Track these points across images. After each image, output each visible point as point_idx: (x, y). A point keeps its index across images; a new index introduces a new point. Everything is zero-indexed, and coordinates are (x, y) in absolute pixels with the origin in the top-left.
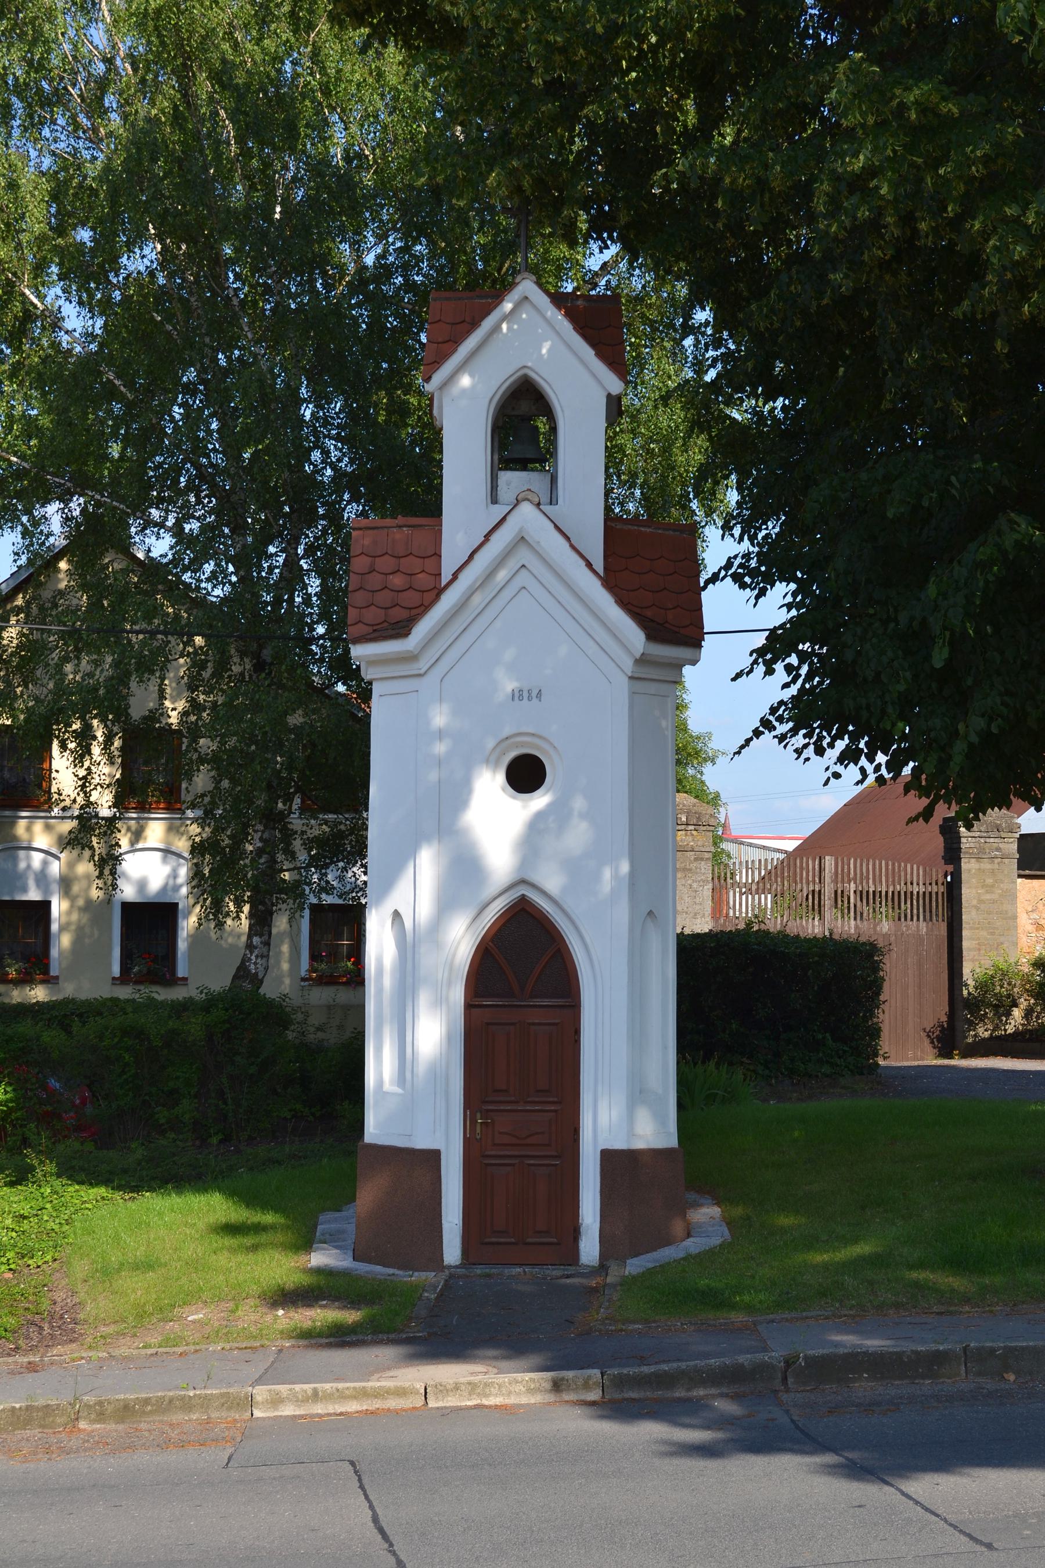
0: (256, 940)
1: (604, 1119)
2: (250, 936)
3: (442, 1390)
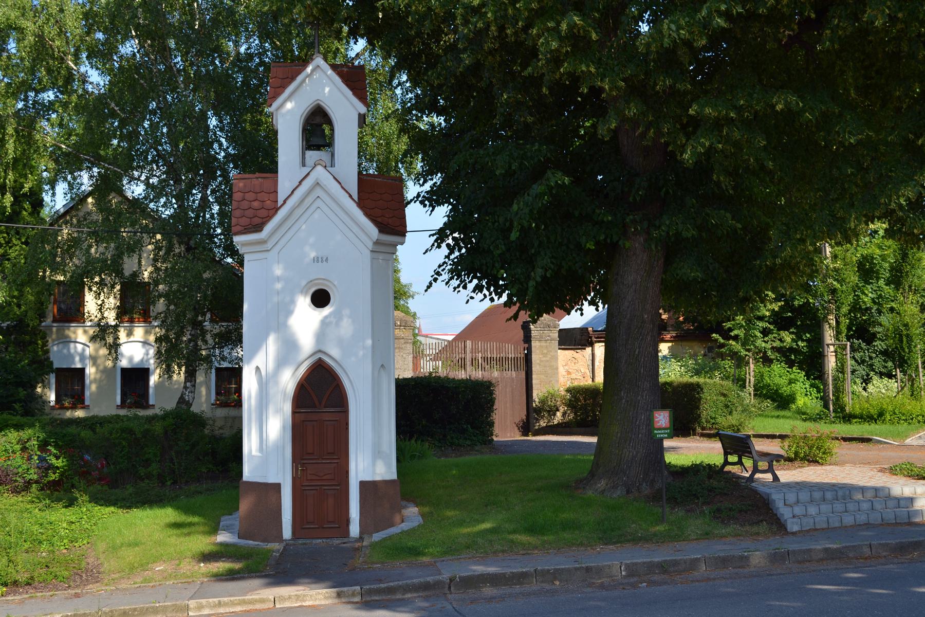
0: (188, 384)
1: (361, 466)
2: (185, 382)
3: (283, 599)
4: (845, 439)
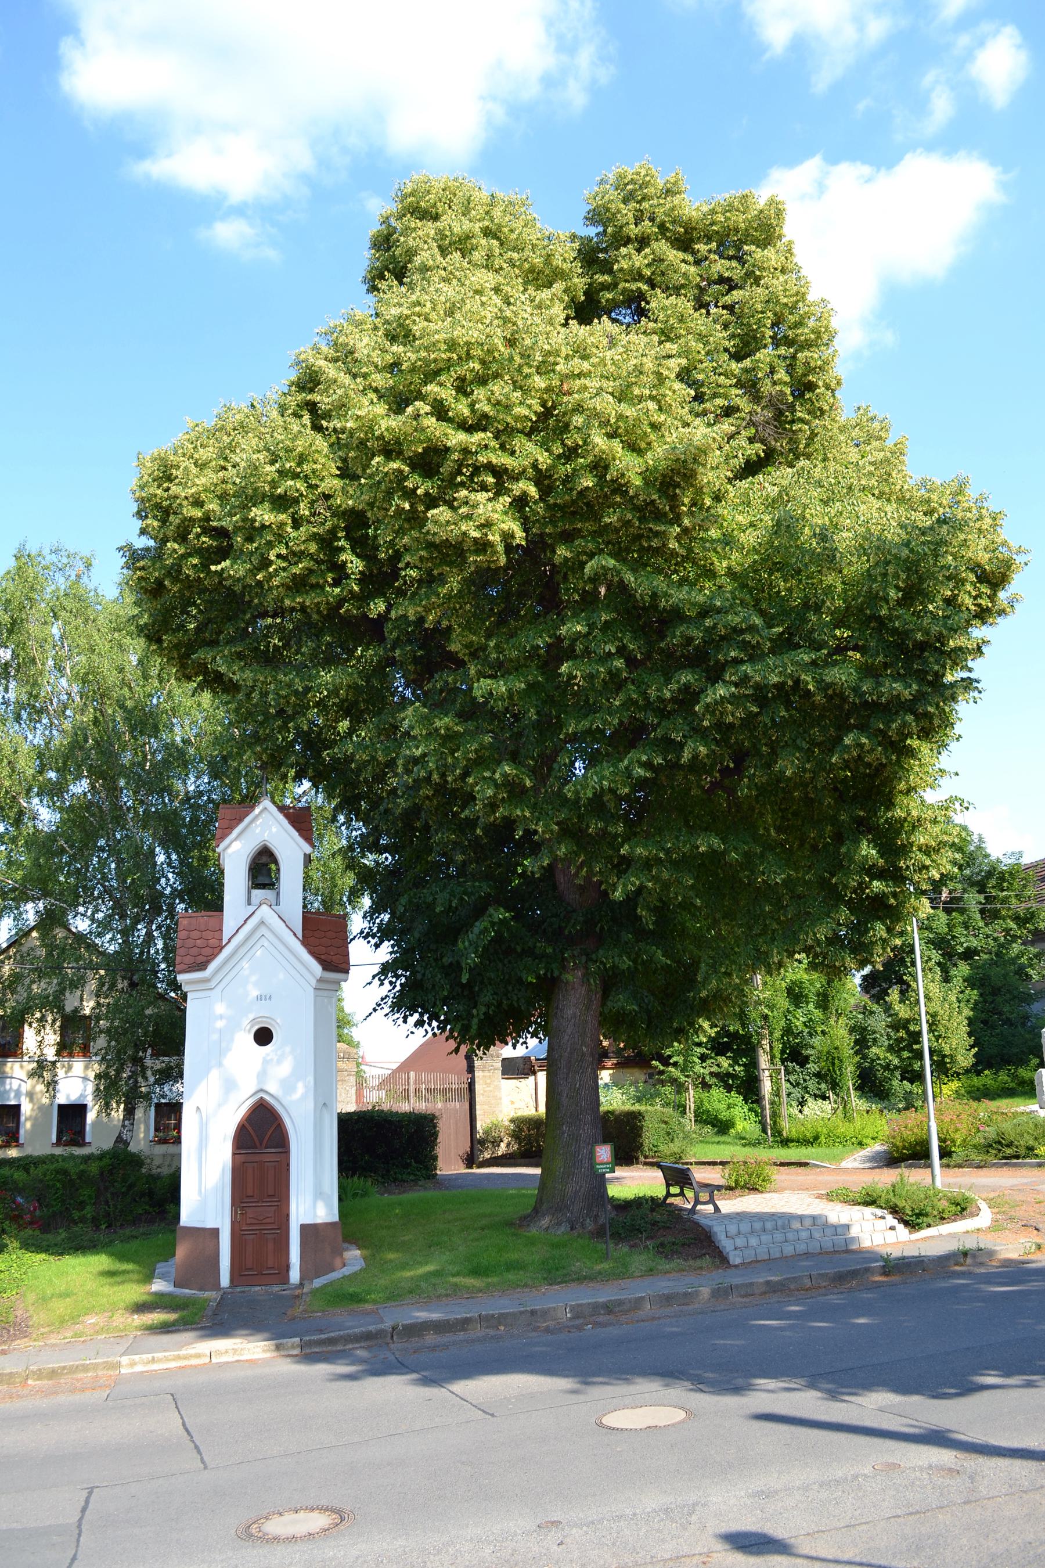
0: (127, 1122)
1: (301, 1209)
2: (124, 1121)
3: (219, 1353)
4: (782, 1164)
